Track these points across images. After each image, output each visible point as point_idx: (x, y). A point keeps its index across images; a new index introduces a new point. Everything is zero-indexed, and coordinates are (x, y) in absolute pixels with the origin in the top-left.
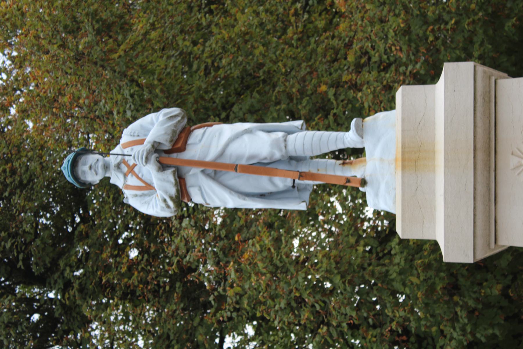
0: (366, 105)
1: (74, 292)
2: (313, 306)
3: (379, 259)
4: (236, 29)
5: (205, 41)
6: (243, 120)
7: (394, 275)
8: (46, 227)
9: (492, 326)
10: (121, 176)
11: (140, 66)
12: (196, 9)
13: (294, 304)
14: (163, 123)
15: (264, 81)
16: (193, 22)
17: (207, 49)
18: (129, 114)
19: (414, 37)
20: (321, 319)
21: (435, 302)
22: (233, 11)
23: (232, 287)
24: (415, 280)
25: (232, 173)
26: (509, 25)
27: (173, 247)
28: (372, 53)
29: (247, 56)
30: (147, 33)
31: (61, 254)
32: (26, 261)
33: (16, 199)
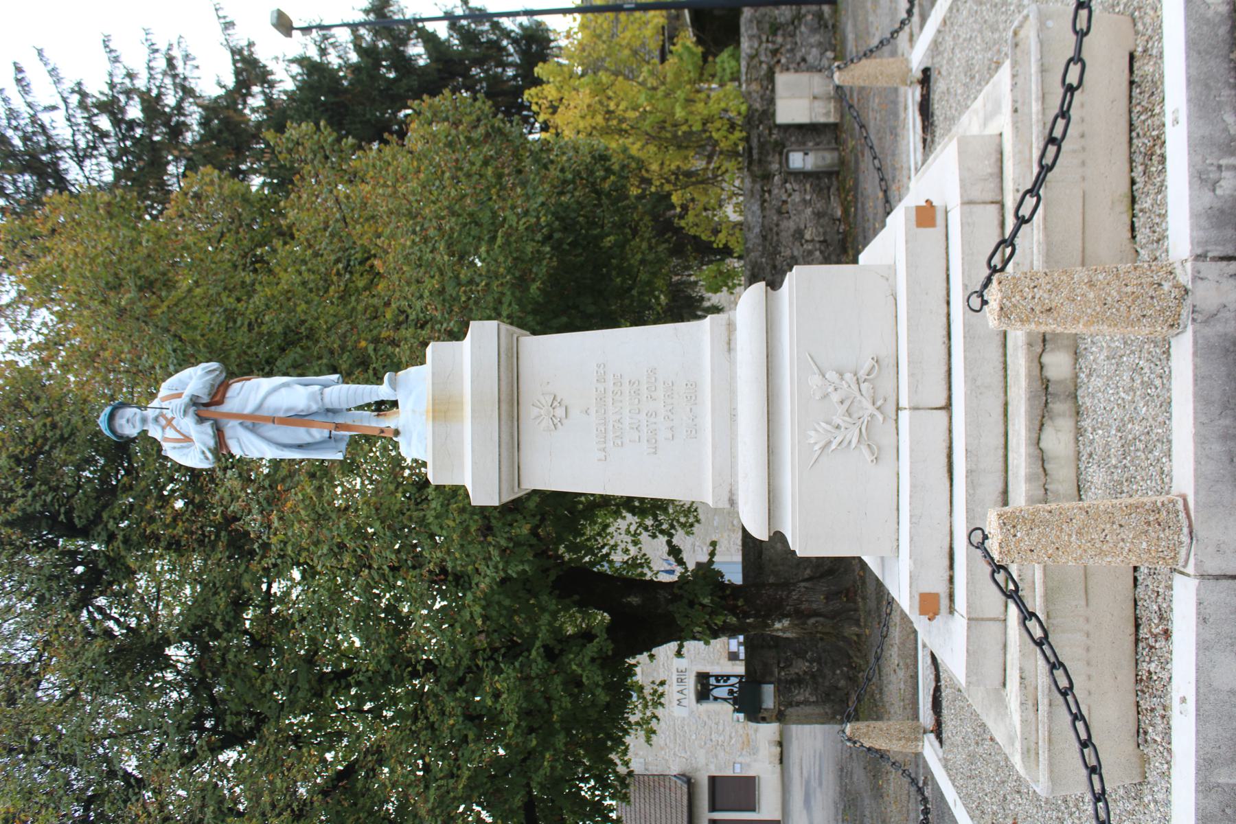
0: (404, 360)
1: (118, 543)
2: (355, 551)
3: (417, 504)
4: (280, 287)
5: (250, 297)
6: (286, 374)
7: (431, 519)
8: (89, 480)
9: (522, 562)
10: (159, 429)
11: (184, 322)
12: (240, 267)
13: (336, 550)
14: (201, 377)
15: (307, 337)
16: (237, 280)
17: (251, 306)
18: (171, 368)
19: (448, 297)
20: (363, 562)
21: (470, 543)
22: (277, 269)
23: (275, 534)
24: (452, 524)
25: (271, 425)
26: (534, 288)
27: (217, 497)
28: (409, 311)
29: (289, 313)
30: (190, 290)
31: (104, 507)
32: (69, 513)
33: (56, 453)
